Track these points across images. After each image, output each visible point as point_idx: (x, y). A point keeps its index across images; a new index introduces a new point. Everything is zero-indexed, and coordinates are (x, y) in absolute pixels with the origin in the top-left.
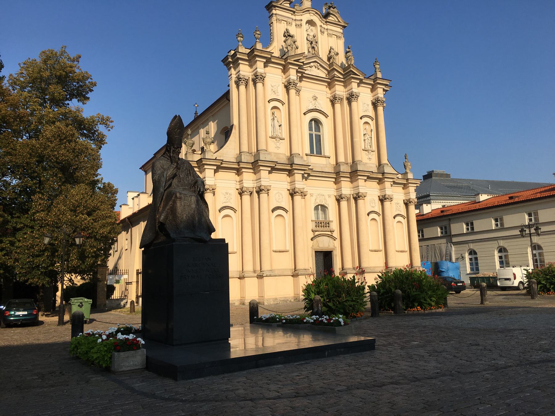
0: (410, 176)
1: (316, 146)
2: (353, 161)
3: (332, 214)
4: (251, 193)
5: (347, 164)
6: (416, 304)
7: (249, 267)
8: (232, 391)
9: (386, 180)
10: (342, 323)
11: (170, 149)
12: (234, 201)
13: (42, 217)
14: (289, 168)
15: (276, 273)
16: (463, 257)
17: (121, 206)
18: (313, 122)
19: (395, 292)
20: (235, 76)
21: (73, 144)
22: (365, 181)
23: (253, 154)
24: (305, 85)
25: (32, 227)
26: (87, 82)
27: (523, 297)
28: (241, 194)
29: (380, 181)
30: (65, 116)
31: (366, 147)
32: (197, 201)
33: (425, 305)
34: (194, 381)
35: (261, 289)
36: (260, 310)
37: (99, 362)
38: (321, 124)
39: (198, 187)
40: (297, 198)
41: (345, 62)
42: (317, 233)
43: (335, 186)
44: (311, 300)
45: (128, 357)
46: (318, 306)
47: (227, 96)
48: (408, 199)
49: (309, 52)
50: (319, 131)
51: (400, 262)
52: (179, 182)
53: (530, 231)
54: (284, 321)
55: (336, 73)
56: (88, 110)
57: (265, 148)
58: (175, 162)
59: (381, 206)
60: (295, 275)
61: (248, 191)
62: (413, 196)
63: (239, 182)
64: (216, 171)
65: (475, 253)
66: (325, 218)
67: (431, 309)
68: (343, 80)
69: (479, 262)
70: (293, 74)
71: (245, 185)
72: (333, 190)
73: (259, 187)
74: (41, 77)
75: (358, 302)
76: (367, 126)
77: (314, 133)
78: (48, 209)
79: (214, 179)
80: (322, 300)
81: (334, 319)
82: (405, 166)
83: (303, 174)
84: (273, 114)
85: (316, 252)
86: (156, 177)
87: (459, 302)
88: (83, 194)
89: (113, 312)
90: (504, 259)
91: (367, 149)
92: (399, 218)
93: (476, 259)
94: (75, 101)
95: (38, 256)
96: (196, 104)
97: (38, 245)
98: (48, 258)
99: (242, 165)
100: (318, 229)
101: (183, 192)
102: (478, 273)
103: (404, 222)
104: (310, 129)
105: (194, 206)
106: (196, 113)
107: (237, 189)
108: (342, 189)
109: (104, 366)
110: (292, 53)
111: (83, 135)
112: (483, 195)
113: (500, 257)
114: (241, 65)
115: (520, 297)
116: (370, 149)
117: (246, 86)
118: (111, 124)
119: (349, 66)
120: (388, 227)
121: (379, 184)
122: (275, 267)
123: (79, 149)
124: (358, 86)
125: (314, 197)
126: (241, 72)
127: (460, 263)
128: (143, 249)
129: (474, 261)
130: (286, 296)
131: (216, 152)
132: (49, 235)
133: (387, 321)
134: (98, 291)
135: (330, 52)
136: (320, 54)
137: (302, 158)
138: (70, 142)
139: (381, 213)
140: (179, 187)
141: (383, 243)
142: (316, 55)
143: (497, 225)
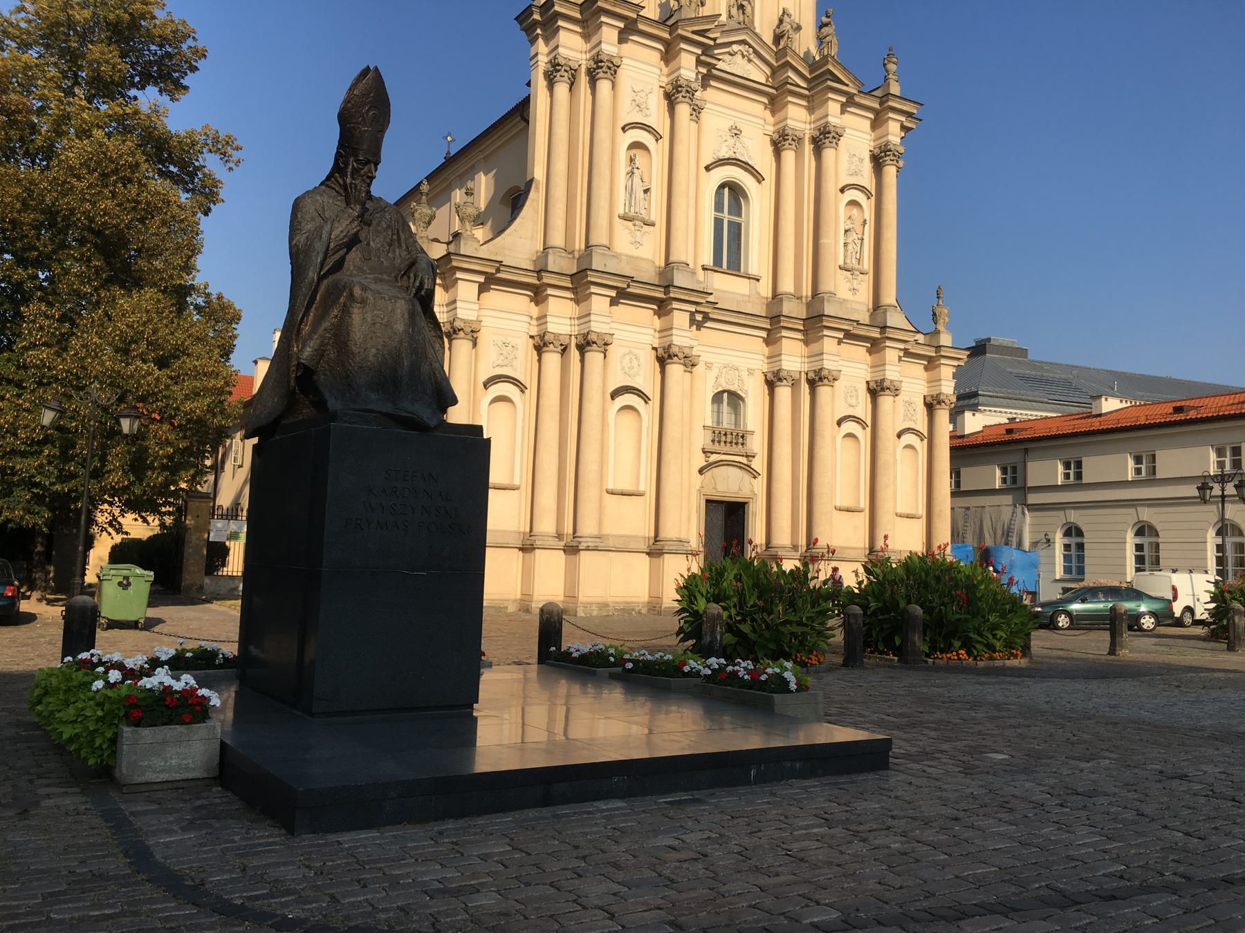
0: (946, 339)
1: (729, 249)
2: (815, 293)
3: (754, 416)
4: (564, 350)
5: (800, 298)
6: (957, 644)
7: (546, 525)
8: (457, 893)
9: (888, 343)
10: (793, 686)
11: (346, 165)
12: (522, 366)
13: (42, 360)
14: (661, 294)
15: (611, 543)
16: (1048, 541)
17: (256, 362)
18: (726, 190)
19: (905, 611)
20: (546, 59)
21: (133, 189)
22: (840, 342)
23: (577, 255)
24: (713, 97)
25: (19, 385)
26: (184, 47)
27: (1205, 644)
28: (539, 349)
29: (875, 346)
30: (123, 124)
31: (848, 261)
32: (412, 315)
33: (978, 646)
34: (347, 839)
35: (527, 575)
36: (566, 629)
37: (78, 750)
38: (745, 196)
39: (416, 276)
40: (675, 370)
41: (814, 51)
42: (714, 458)
43: (766, 350)
44: (696, 614)
45: (164, 742)
46: (713, 632)
47: (522, 110)
48: (934, 393)
49: (730, 16)
50: (740, 215)
51: (905, 541)
52: (366, 259)
53: (1223, 490)
54: (630, 666)
55: (791, 74)
56: (179, 116)
57: (605, 242)
58: (357, 202)
59: (870, 406)
60: (656, 550)
61: (557, 343)
62: (948, 388)
63: (538, 319)
64: (483, 288)
65: (1080, 533)
66: (737, 423)
67: (991, 658)
68: (806, 92)
69: (1086, 553)
70: (687, 67)
71: (552, 328)
72: (762, 357)
73: (586, 335)
74: (71, 24)
75: (813, 628)
76: (855, 211)
77: (726, 217)
78: (61, 344)
79: (477, 307)
80: (725, 614)
81: (769, 670)
82: (934, 314)
83: (692, 314)
84: (632, 160)
85: (708, 501)
86: (301, 239)
87: (1048, 645)
88: (147, 312)
89: (215, 606)
90: (1146, 553)
91: (849, 266)
92: (909, 439)
93: (1081, 547)
94: (152, 91)
95: (24, 454)
96: (449, 134)
97: (26, 427)
98: (50, 463)
99: (547, 279)
100: (716, 447)
101: (373, 286)
102: (1083, 580)
103: (922, 447)
104: (719, 207)
105: (400, 327)
106: (448, 153)
107: (532, 337)
108: (783, 357)
109: (91, 762)
110: (688, 13)
111: (165, 174)
112: (1111, 400)
113: (1139, 547)
114: (562, 32)
115: (1192, 643)
116: (856, 266)
117: (572, 84)
118: (236, 155)
119: (825, 60)
120: (883, 457)
121: (870, 352)
122: (608, 530)
123: (148, 204)
124: (843, 112)
125: (715, 372)
126: (561, 50)
127: (1042, 553)
128: (255, 440)
129: (1073, 551)
130: (628, 600)
131: (486, 243)
132: (54, 404)
133: (882, 681)
134: (186, 554)
135: (781, 21)
136: (757, 24)
137: (694, 273)
138: (127, 181)
139: (869, 423)
140: (364, 272)
141: (869, 493)
142: (748, 27)
143: (1138, 471)
